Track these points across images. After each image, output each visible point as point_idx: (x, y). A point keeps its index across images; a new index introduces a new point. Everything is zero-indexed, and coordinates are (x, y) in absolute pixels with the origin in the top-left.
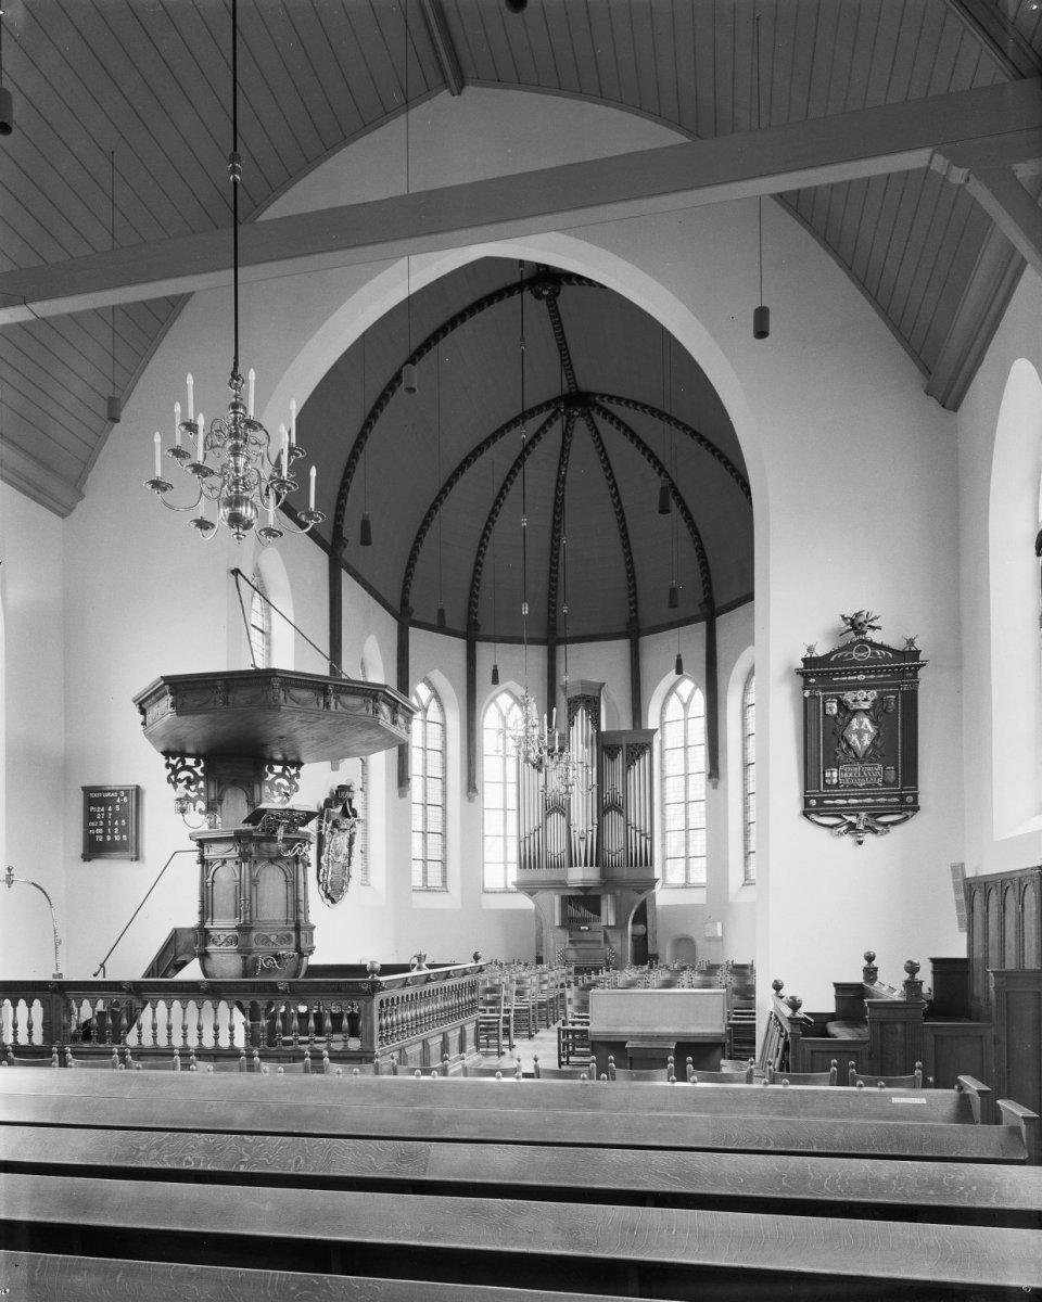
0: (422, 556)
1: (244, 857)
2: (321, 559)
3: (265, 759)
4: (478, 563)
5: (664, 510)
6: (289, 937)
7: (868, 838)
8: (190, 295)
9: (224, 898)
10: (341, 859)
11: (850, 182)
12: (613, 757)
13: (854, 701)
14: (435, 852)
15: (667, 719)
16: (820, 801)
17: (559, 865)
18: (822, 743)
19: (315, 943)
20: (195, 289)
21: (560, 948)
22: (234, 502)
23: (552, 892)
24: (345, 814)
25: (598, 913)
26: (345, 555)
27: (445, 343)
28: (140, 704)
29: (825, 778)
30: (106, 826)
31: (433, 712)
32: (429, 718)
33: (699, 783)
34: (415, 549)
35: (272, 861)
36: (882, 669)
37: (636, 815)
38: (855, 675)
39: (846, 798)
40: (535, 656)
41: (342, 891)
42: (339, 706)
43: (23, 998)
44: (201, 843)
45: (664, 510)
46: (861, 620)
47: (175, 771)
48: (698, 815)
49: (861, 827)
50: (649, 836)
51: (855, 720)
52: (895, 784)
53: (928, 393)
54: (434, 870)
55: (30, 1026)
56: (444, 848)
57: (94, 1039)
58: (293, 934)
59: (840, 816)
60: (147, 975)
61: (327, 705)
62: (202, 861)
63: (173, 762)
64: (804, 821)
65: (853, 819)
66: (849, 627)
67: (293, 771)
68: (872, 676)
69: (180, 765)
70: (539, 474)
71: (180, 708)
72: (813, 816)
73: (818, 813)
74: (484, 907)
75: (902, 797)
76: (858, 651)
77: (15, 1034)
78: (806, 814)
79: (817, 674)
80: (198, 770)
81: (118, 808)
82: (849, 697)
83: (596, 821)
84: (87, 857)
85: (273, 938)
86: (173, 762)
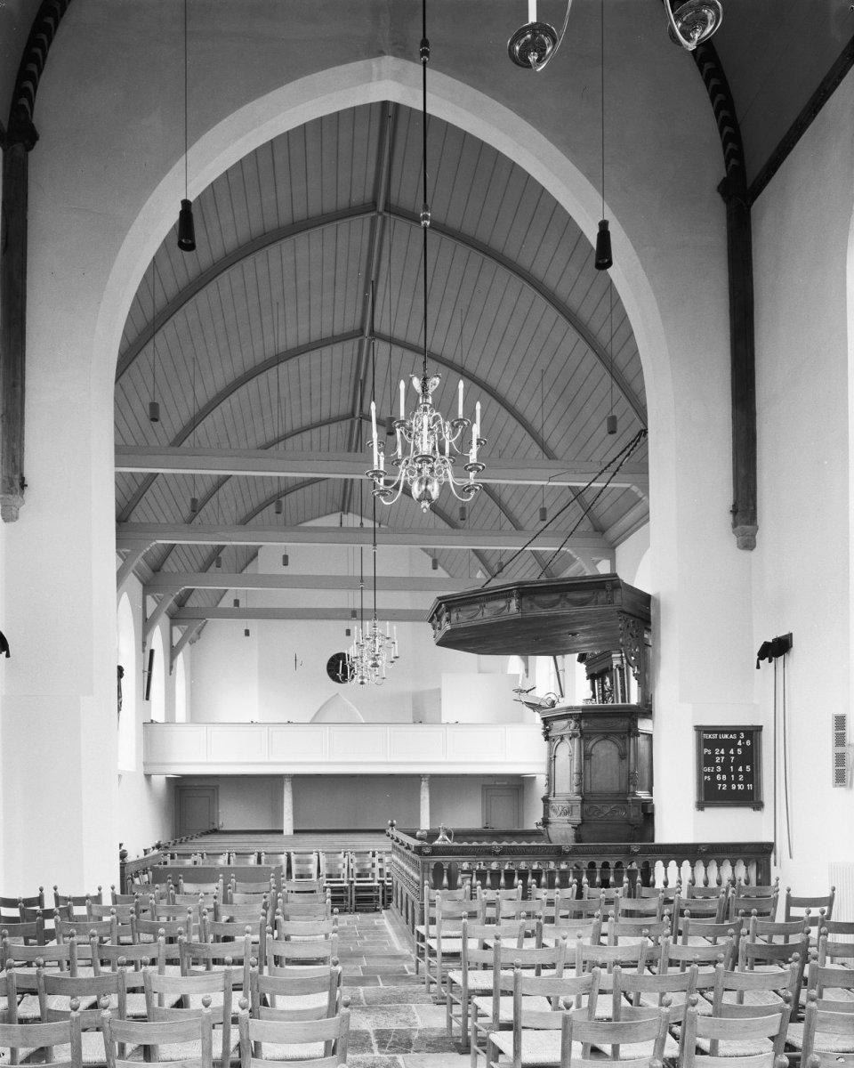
43: (662, 860)
81: (739, 751)
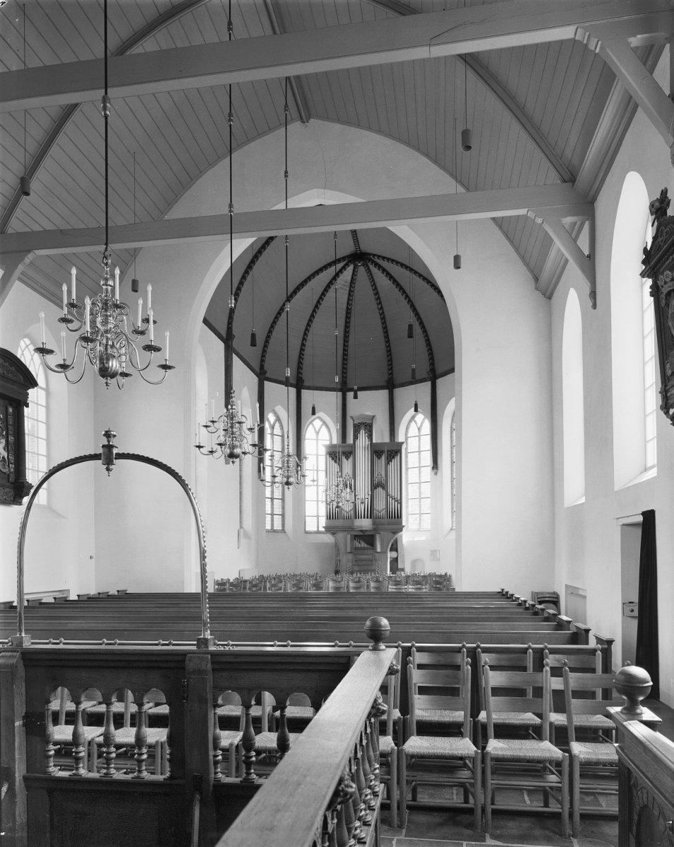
2: (220, 346)
4: (303, 345)
15: (409, 436)
33: (428, 471)
37: (392, 490)
40: (333, 398)
48: (426, 490)
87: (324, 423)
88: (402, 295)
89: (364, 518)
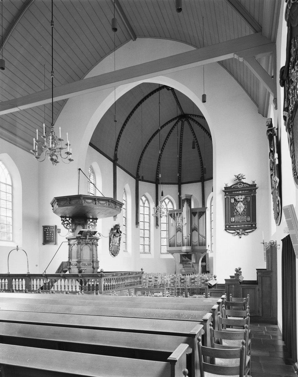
0: (143, 161)
1: (79, 243)
2: (111, 164)
3: (87, 218)
5: (194, 148)
6: (91, 264)
7: (243, 236)
8: (68, 99)
9: (74, 254)
10: (117, 244)
11: (229, 59)
12: (195, 215)
13: (238, 199)
14: (147, 242)
16: (229, 226)
17: (181, 246)
18: (230, 210)
19: (99, 266)
20: (69, 98)
21: (180, 269)
22: (52, 155)
23: (178, 253)
24: (117, 232)
25: (191, 259)
26: (118, 162)
27: (143, 104)
28: (52, 204)
29: (231, 220)
30: (48, 235)
31: (146, 204)
32: (145, 206)
34: (140, 160)
35: (86, 244)
36: (246, 190)
37: (201, 232)
38: (239, 191)
39: (237, 225)
40: (175, 188)
41: (117, 253)
42: (85, 202)
44: (69, 240)
45: (194, 148)
46: (240, 176)
47: (64, 221)
49: (240, 233)
50: (205, 237)
51: (239, 204)
52: (250, 221)
53: (259, 113)
54: (147, 248)
55: (22, 286)
56: (150, 242)
57: (47, 289)
58: (92, 263)
59: (235, 230)
60: (57, 272)
61: (96, 203)
62: (69, 244)
63: (63, 219)
64: (225, 231)
65: (238, 231)
66: (237, 178)
67: (95, 221)
68: (243, 192)
69: (65, 220)
70: (175, 138)
71: (59, 205)
72: (227, 230)
73: (229, 230)
74: (161, 258)
75: (252, 225)
76: (239, 185)
77: (19, 287)
78: (226, 230)
79: (229, 191)
80: (70, 221)
82: (237, 197)
83: (190, 234)
84: (44, 244)
85: (86, 264)
86: (63, 219)
87: (170, 200)
88: (205, 132)
89: (203, 246)
